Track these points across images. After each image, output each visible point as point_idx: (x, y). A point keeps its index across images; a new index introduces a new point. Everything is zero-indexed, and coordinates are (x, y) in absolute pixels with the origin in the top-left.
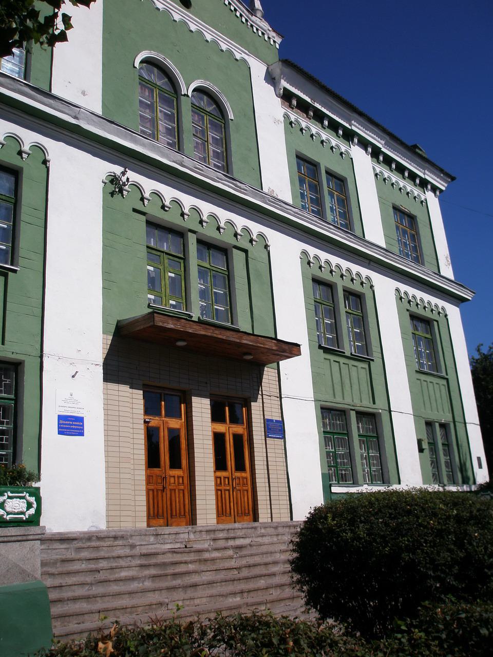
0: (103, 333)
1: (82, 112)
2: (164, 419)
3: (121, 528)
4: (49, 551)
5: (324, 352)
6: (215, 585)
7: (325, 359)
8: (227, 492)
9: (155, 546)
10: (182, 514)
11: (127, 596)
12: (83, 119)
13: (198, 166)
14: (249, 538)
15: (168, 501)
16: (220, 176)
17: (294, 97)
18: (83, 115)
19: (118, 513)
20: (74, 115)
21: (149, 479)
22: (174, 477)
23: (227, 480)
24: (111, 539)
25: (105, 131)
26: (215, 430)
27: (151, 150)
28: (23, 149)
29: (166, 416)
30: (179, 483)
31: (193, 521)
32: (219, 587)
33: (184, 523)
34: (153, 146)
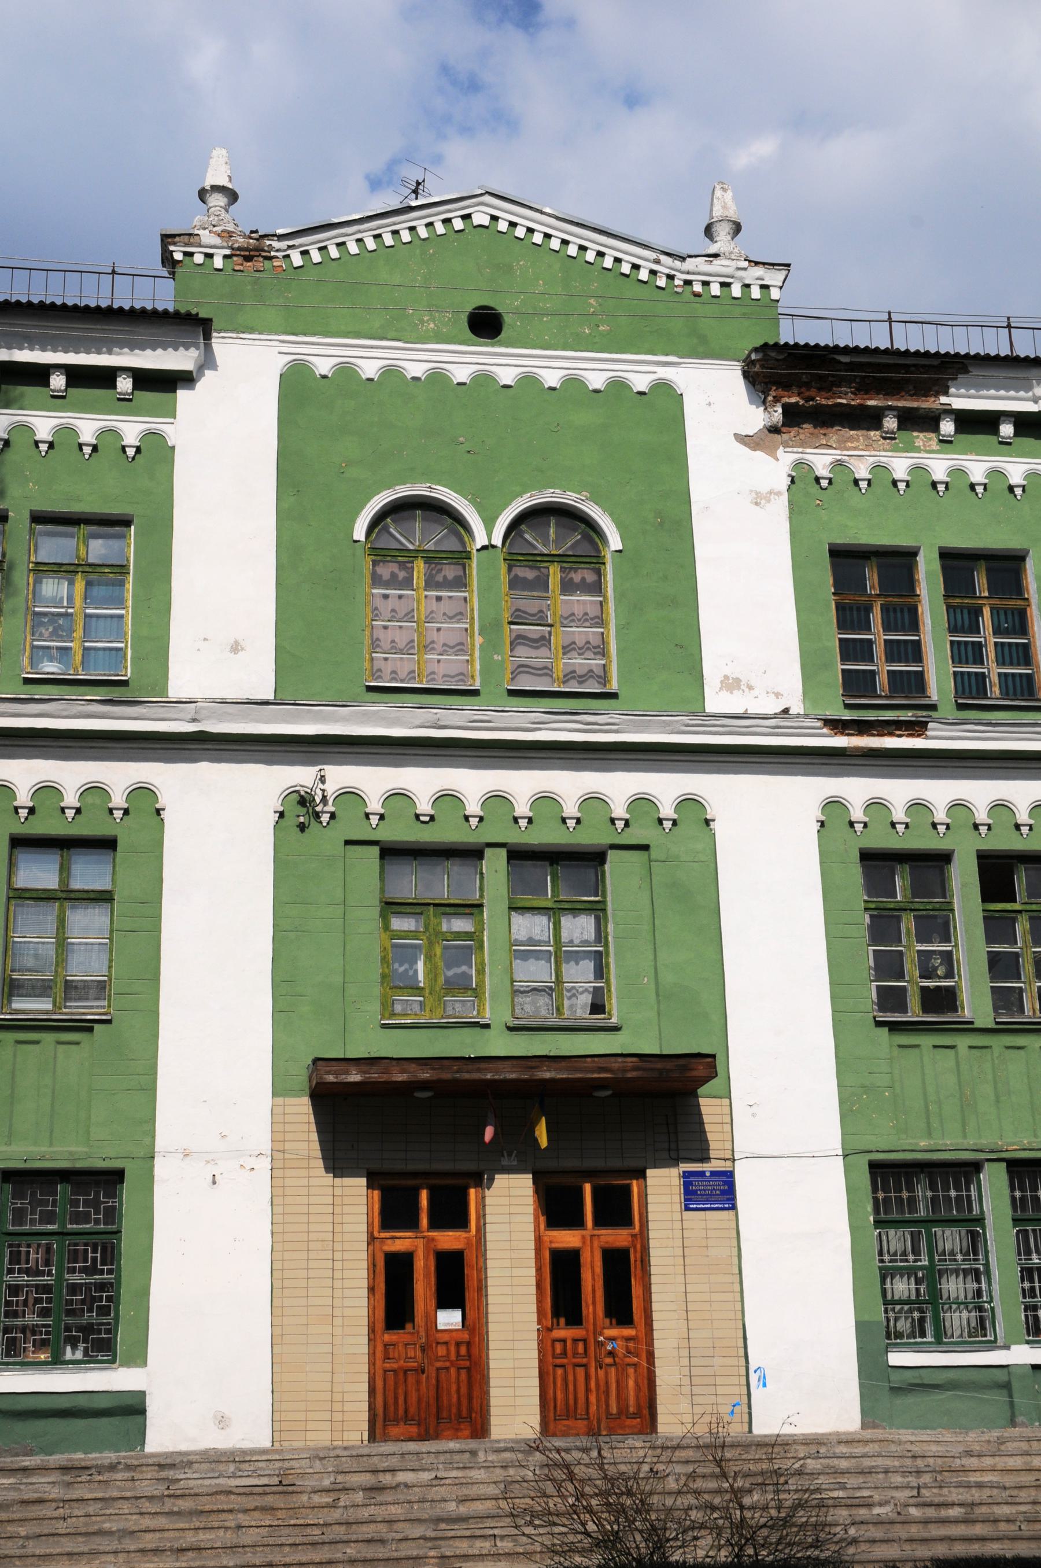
0: (275, 1094)
1: (202, 708)
2: (426, 1234)
3: (308, 1443)
4: (22, 1487)
5: (890, 1030)
6: (240, 1550)
7: (900, 1046)
8: (581, 1371)
9: (217, 1481)
10: (465, 1413)
11: (65, 1558)
12: (208, 718)
13: (476, 717)
14: (429, 1470)
15: (425, 1392)
16: (536, 718)
17: (887, 413)
18: (205, 712)
19: (301, 1416)
20: (190, 716)
21: (379, 1354)
22: (446, 1343)
23: (581, 1345)
24: (153, 1468)
25: (257, 721)
26: (554, 1245)
27: (362, 722)
28: (857, 476)
29: (434, 1225)
30: (458, 1354)
31: (479, 1428)
32: (249, 1555)
33: (467, 1432)
34: (365, 714)
